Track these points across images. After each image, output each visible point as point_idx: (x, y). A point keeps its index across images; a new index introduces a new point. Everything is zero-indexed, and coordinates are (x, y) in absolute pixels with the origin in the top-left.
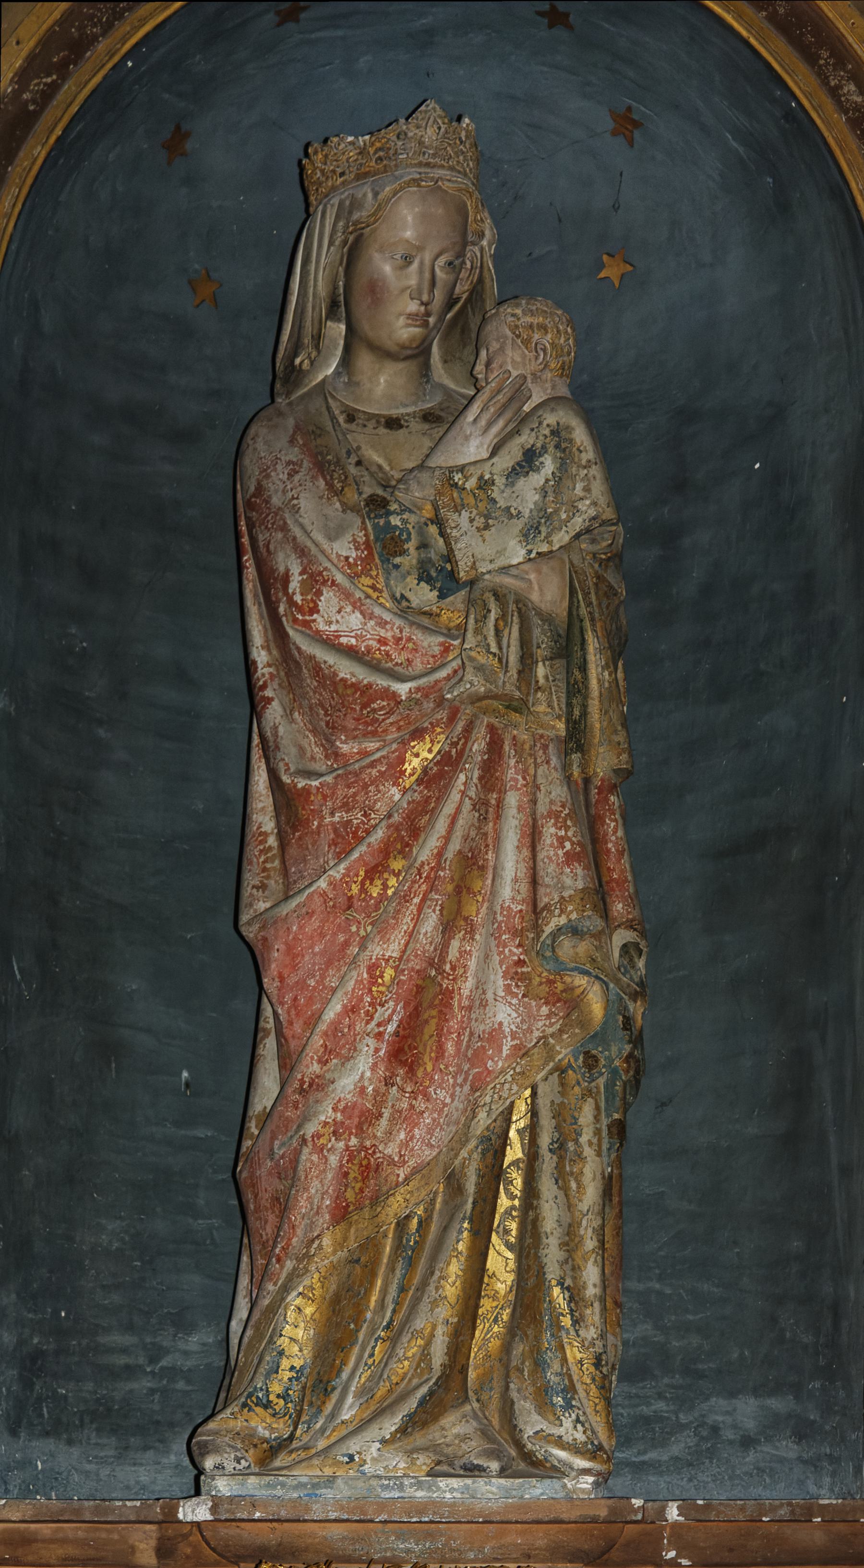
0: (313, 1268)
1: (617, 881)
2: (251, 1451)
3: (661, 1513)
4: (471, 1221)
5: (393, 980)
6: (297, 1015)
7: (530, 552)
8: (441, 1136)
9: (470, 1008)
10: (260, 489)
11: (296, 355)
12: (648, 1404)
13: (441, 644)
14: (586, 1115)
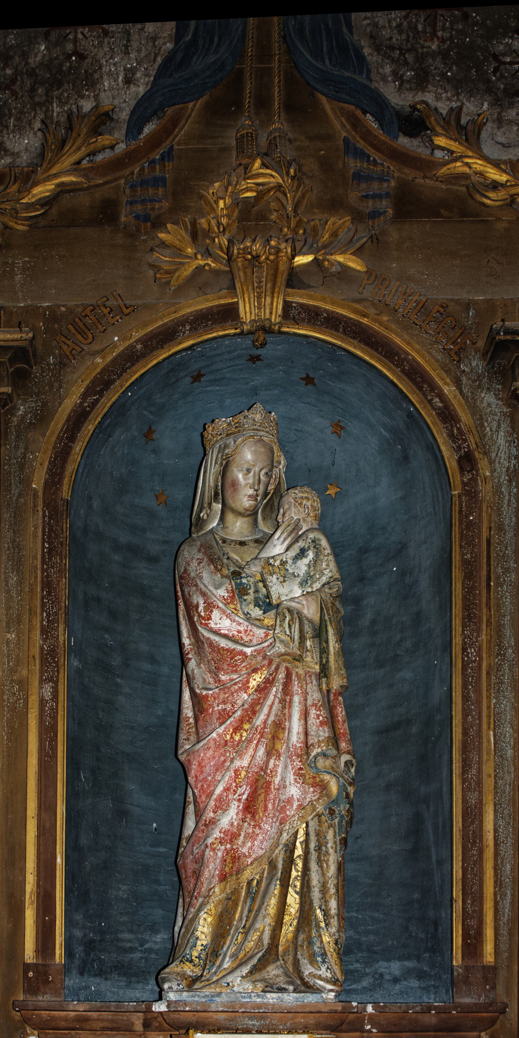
0: (211, 901)
1: (342, 733)
2: (185, 981)
3: (365, 1010)
4: (280, 881)
5: (245, 776)
6: (203, 792)
7: (303, 591)
8: (266, 845)
9: (278, 789)
10: (186, 570)
11: (201, 512)
12: (352, 965)
13: (265, 633)
14: (330, 835)
